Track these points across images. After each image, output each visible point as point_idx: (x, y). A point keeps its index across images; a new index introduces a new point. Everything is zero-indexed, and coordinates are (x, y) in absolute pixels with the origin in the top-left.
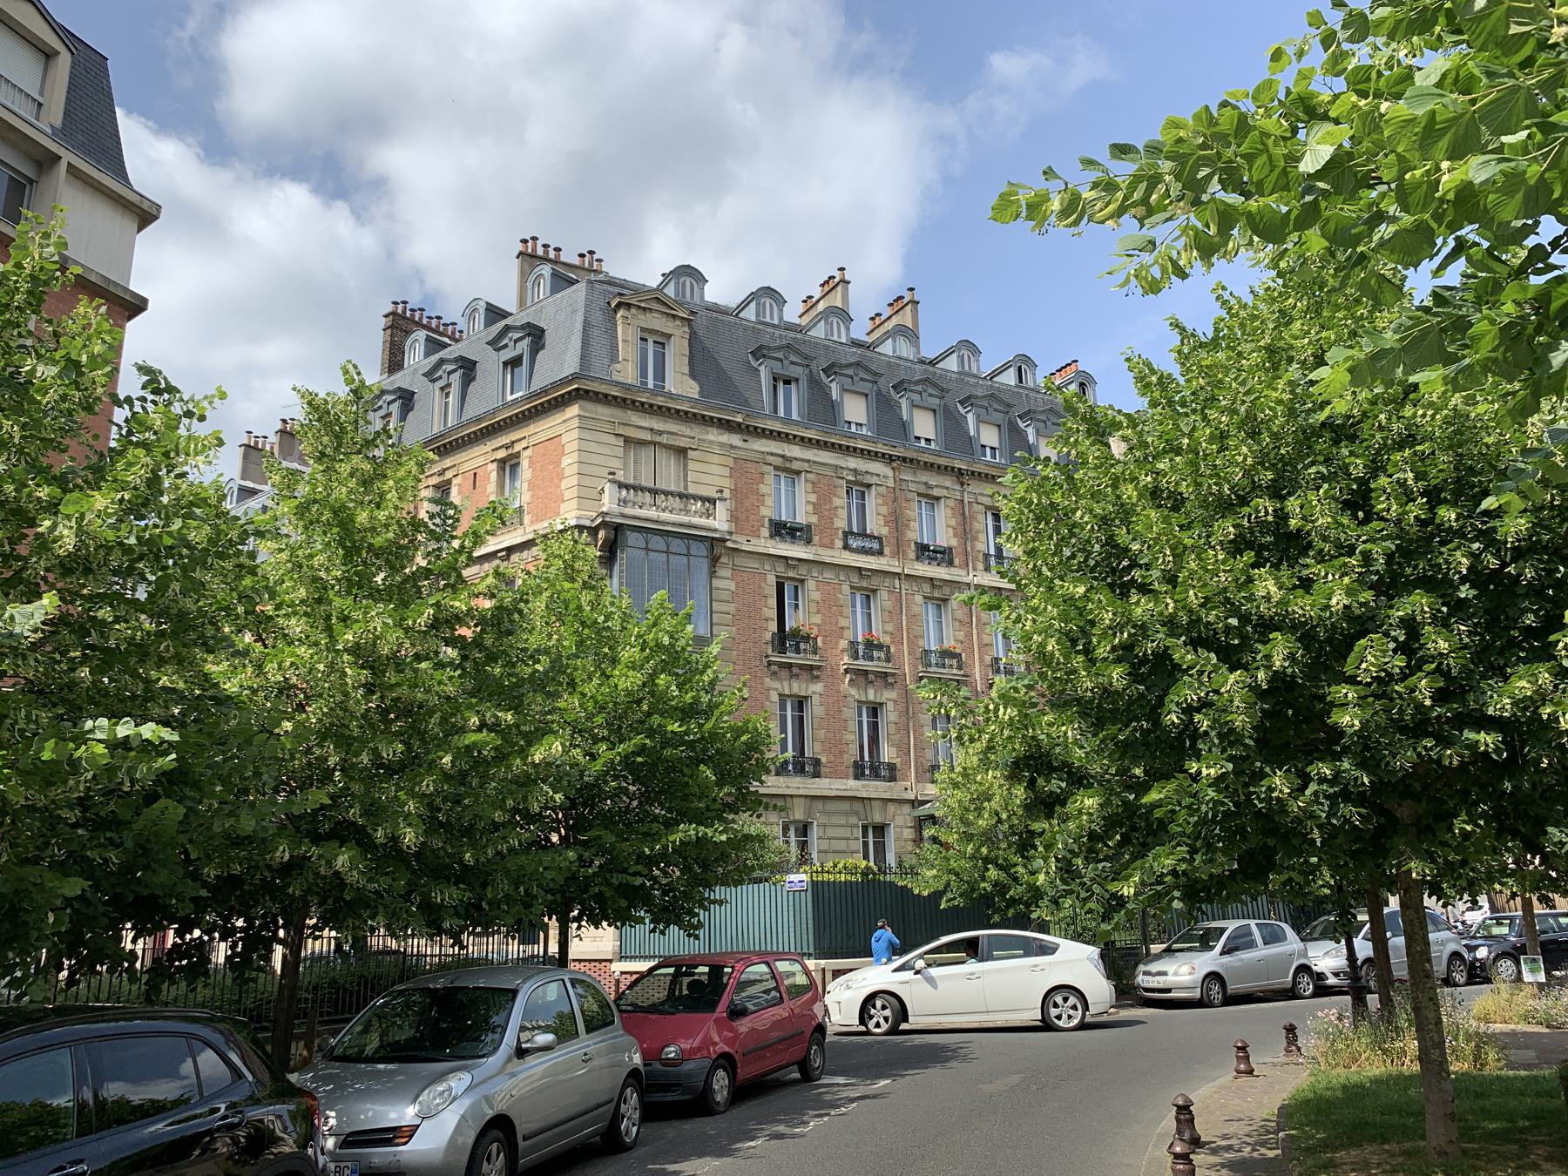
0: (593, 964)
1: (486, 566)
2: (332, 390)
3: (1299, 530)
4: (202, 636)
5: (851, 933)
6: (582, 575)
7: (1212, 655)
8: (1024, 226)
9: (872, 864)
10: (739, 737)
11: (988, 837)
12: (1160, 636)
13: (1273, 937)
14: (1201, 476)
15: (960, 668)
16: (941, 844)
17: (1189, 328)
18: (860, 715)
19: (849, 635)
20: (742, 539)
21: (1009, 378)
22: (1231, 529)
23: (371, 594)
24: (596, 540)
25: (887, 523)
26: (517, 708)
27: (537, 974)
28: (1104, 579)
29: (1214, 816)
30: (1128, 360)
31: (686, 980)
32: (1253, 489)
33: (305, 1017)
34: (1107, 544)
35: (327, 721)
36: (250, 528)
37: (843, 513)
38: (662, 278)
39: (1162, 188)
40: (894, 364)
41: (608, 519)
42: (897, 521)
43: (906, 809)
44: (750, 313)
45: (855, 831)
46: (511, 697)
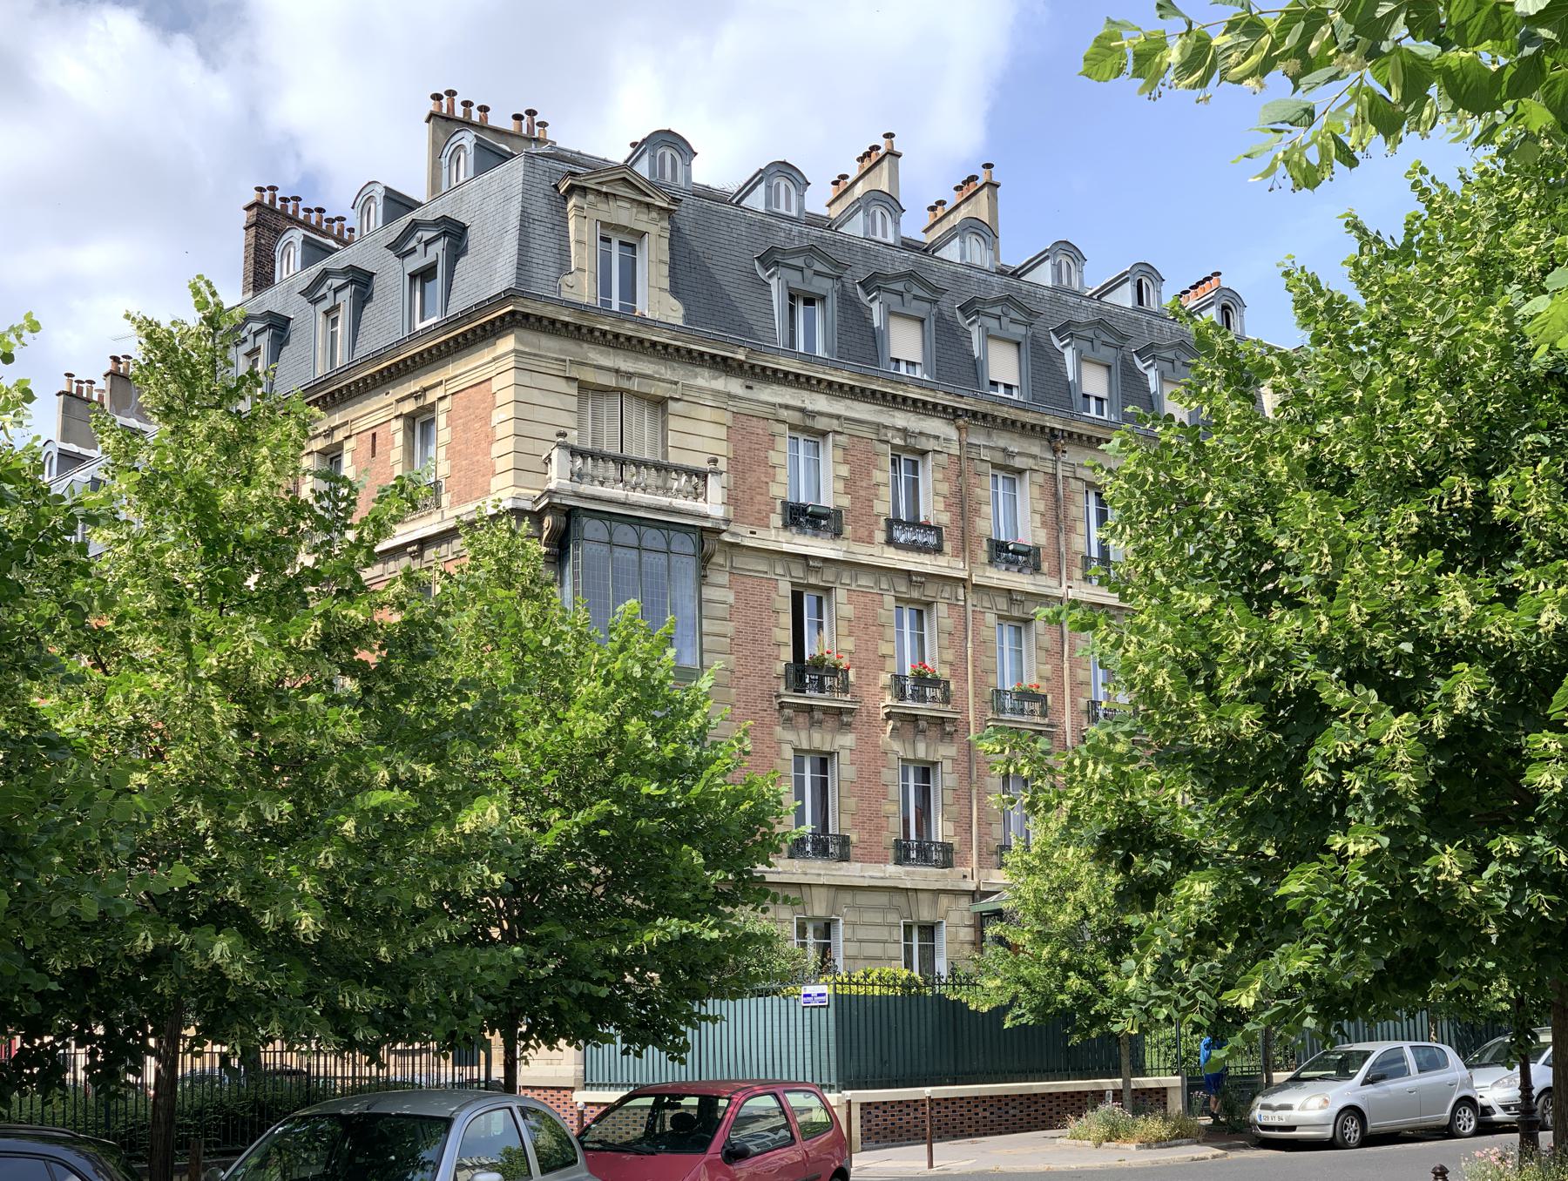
0: (549, 1092)
1: (392, 565)
2: (181, 316)
3: (1505, 522)
4: (20, 657)
5: (886, 1058)
6: (522, 578)
7: (1373, 693)
8: (1129, 84)
9: (916, 974)
10: (737, 805)
11: (1071, 937)
12: (1308, 666)
13: (1431, 1063)
14: (1376, 443)
15: (1044, 715)
16: (1008, 946)
17: (1372, 231)
18: (905, 778)
19: (892, 666)
20: (744, 530)
21: (1124, 297)
22: (1414, 519)
23: (241, 604)
24: (540, 529)
25: (948, 506)
26: (439, 760)
27: (478, 1099)
28: (1239, 588)
29: (1361, 905)
30: (1287, 274)
31: (669, 1114)
32: (1447, 462)
33: (188, 1147)
34: (1245, 539)
35: (192, 773)
36: (77, 511)
37: (886, 493)
38: (631, 150)
39: (1325, 30)
40: (963, 274)
41: (556, 500)
42: (963, 505)
43: (964, 902)
44: (757, 201)
45: (895, 931)
46: (432, 746)
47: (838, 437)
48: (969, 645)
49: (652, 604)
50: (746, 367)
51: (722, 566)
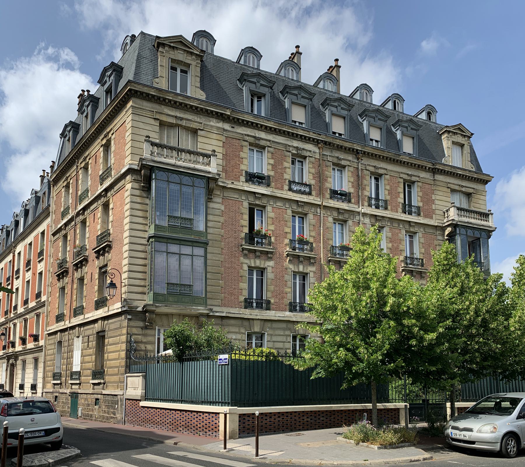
21: (390, 106)
37: (289, 171)
42: (321, 178)
45: (288, 338)
47: (269, 149)
49: (186, 206)
50: (231, 118)
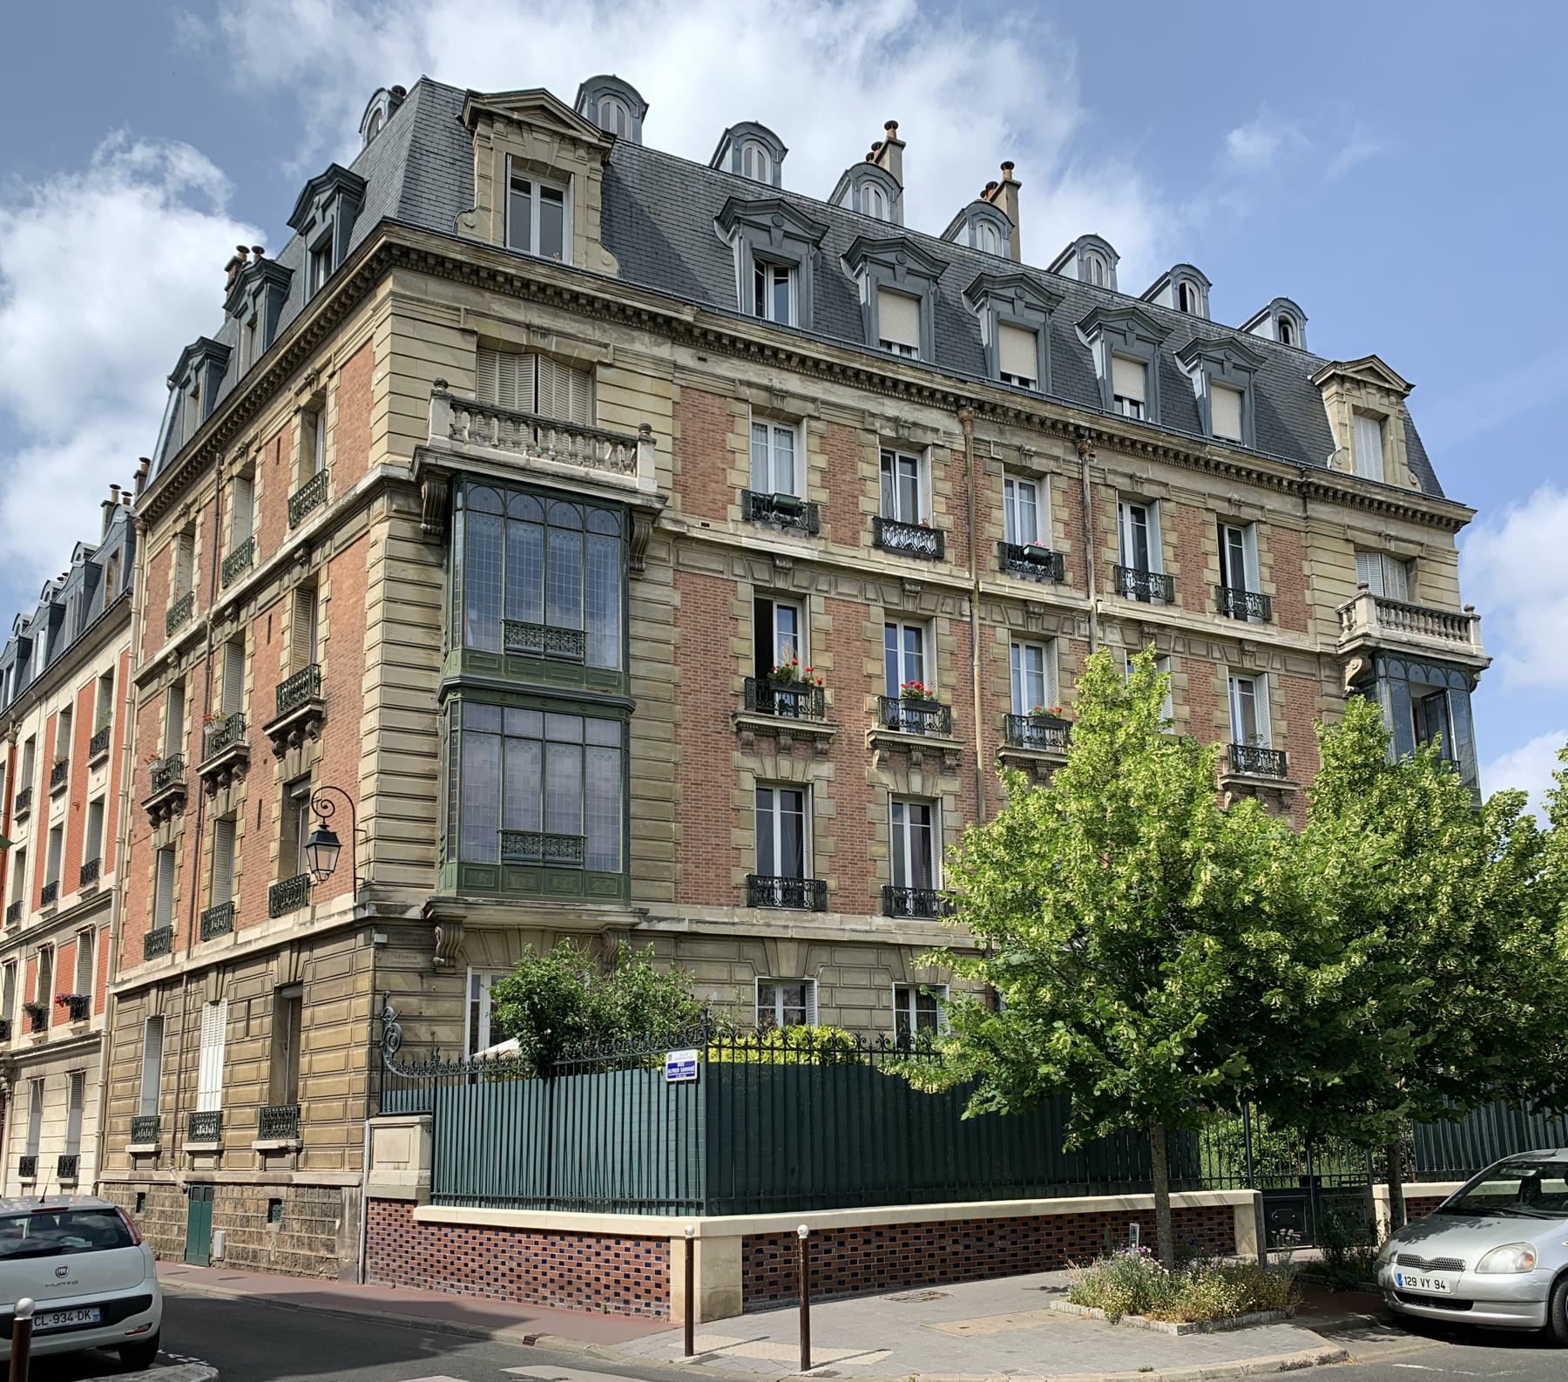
37: (875, 489)
42: (970, 508)
45: (884, 996)
47: (814, 423)
48: (976, 662)
50: (696, 332)
51: (664, 560)
